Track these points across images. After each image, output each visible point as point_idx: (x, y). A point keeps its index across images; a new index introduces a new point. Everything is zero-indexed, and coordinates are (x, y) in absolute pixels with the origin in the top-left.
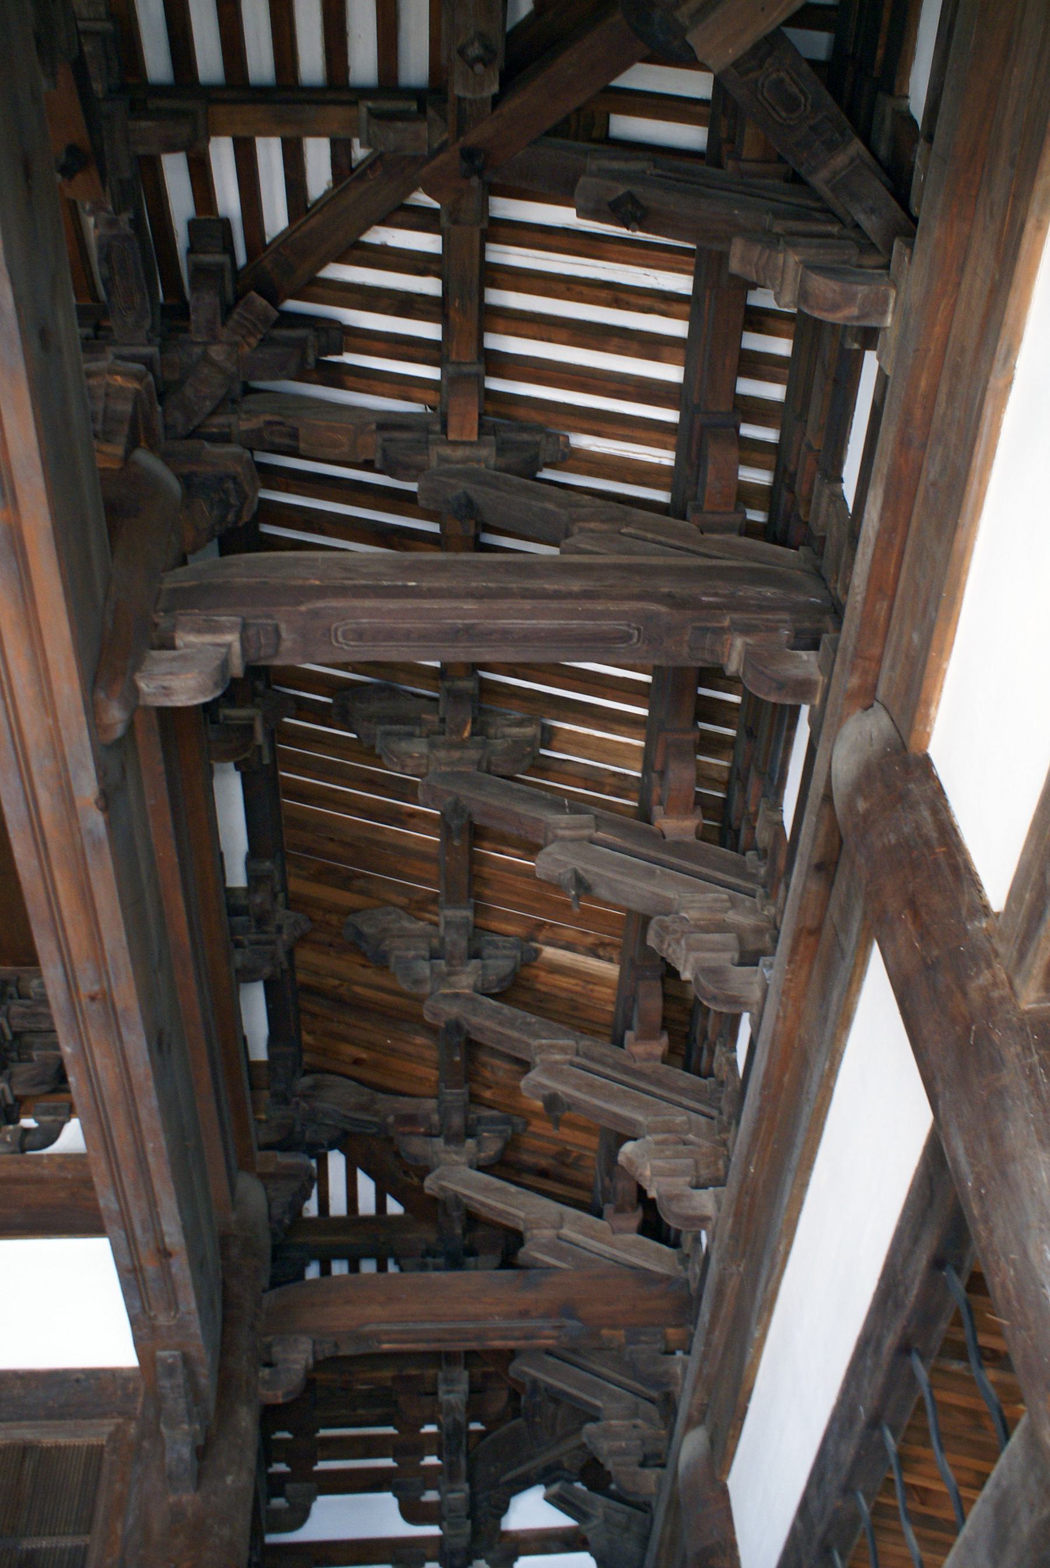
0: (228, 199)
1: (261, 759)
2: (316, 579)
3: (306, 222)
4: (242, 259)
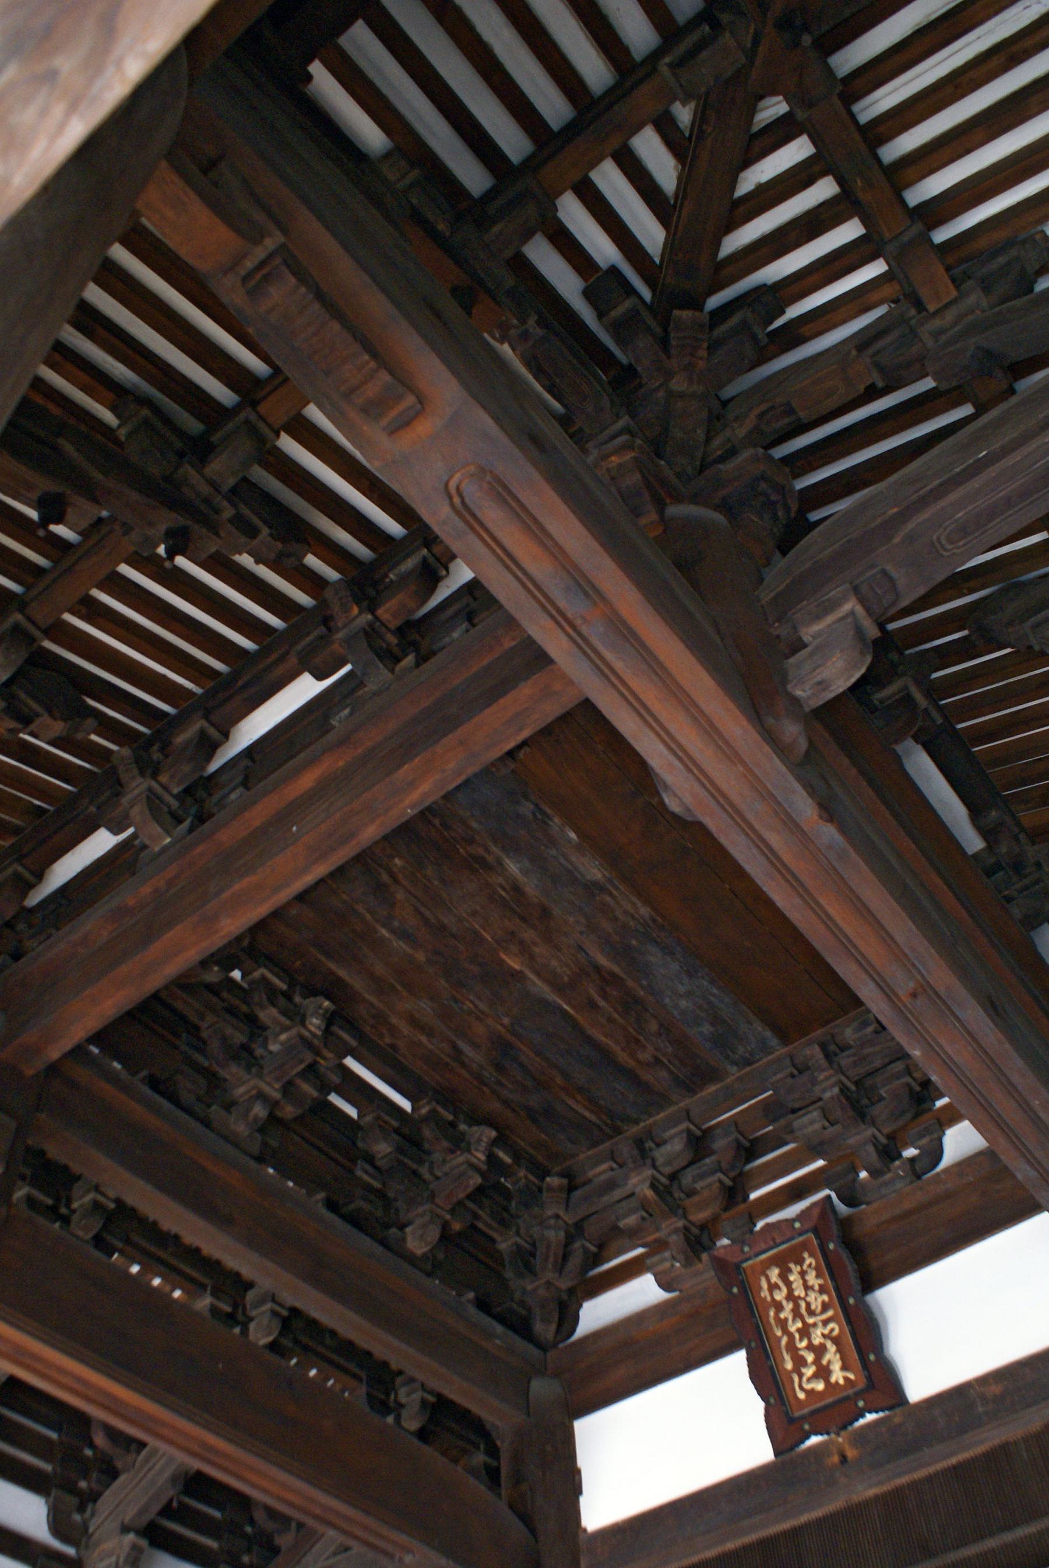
0: (602, 248)
1: (933, 721)
2: (892, 508)
3: (679, 217)
4: (646, 294)
